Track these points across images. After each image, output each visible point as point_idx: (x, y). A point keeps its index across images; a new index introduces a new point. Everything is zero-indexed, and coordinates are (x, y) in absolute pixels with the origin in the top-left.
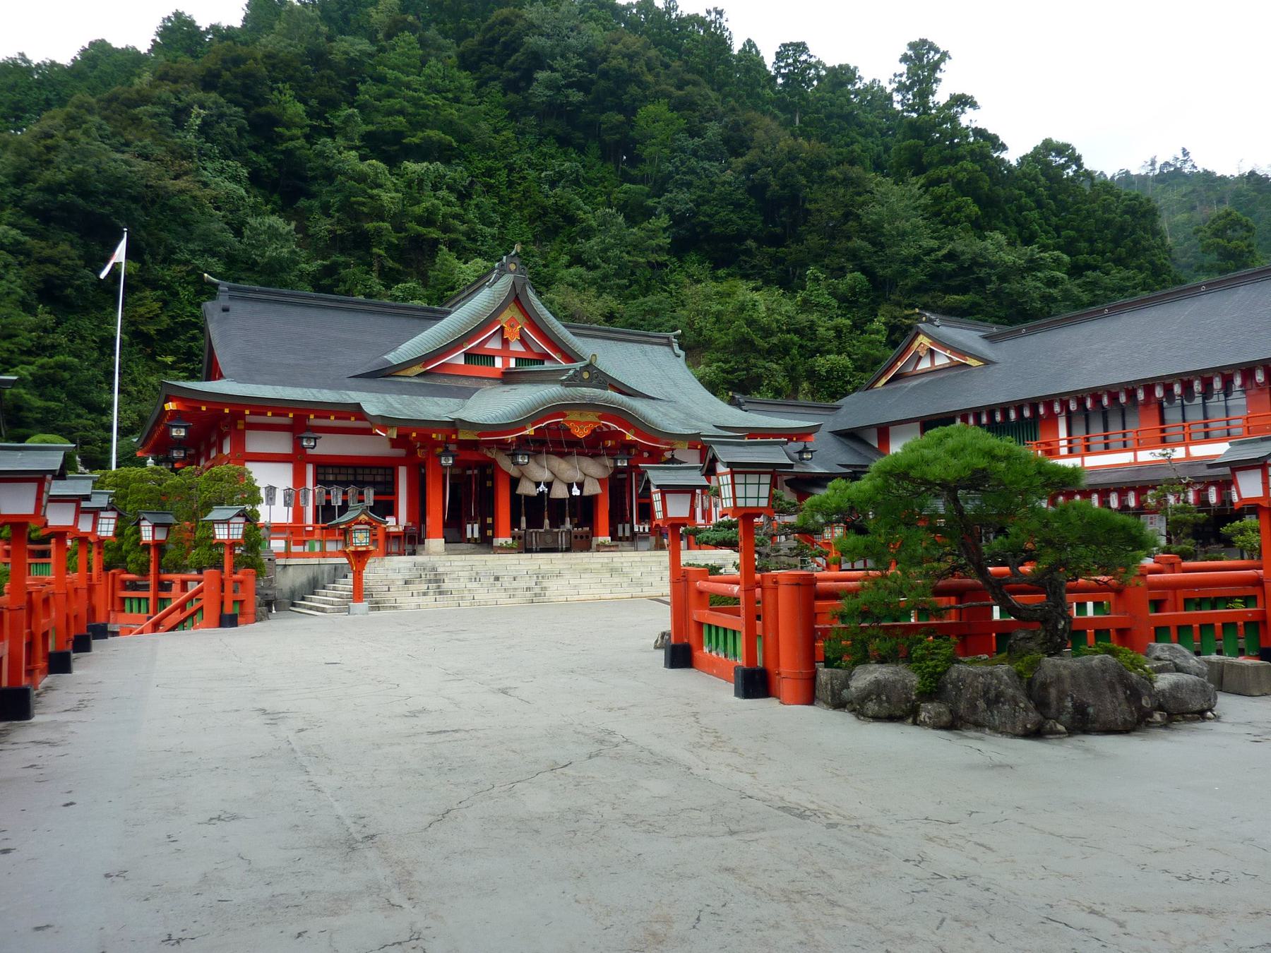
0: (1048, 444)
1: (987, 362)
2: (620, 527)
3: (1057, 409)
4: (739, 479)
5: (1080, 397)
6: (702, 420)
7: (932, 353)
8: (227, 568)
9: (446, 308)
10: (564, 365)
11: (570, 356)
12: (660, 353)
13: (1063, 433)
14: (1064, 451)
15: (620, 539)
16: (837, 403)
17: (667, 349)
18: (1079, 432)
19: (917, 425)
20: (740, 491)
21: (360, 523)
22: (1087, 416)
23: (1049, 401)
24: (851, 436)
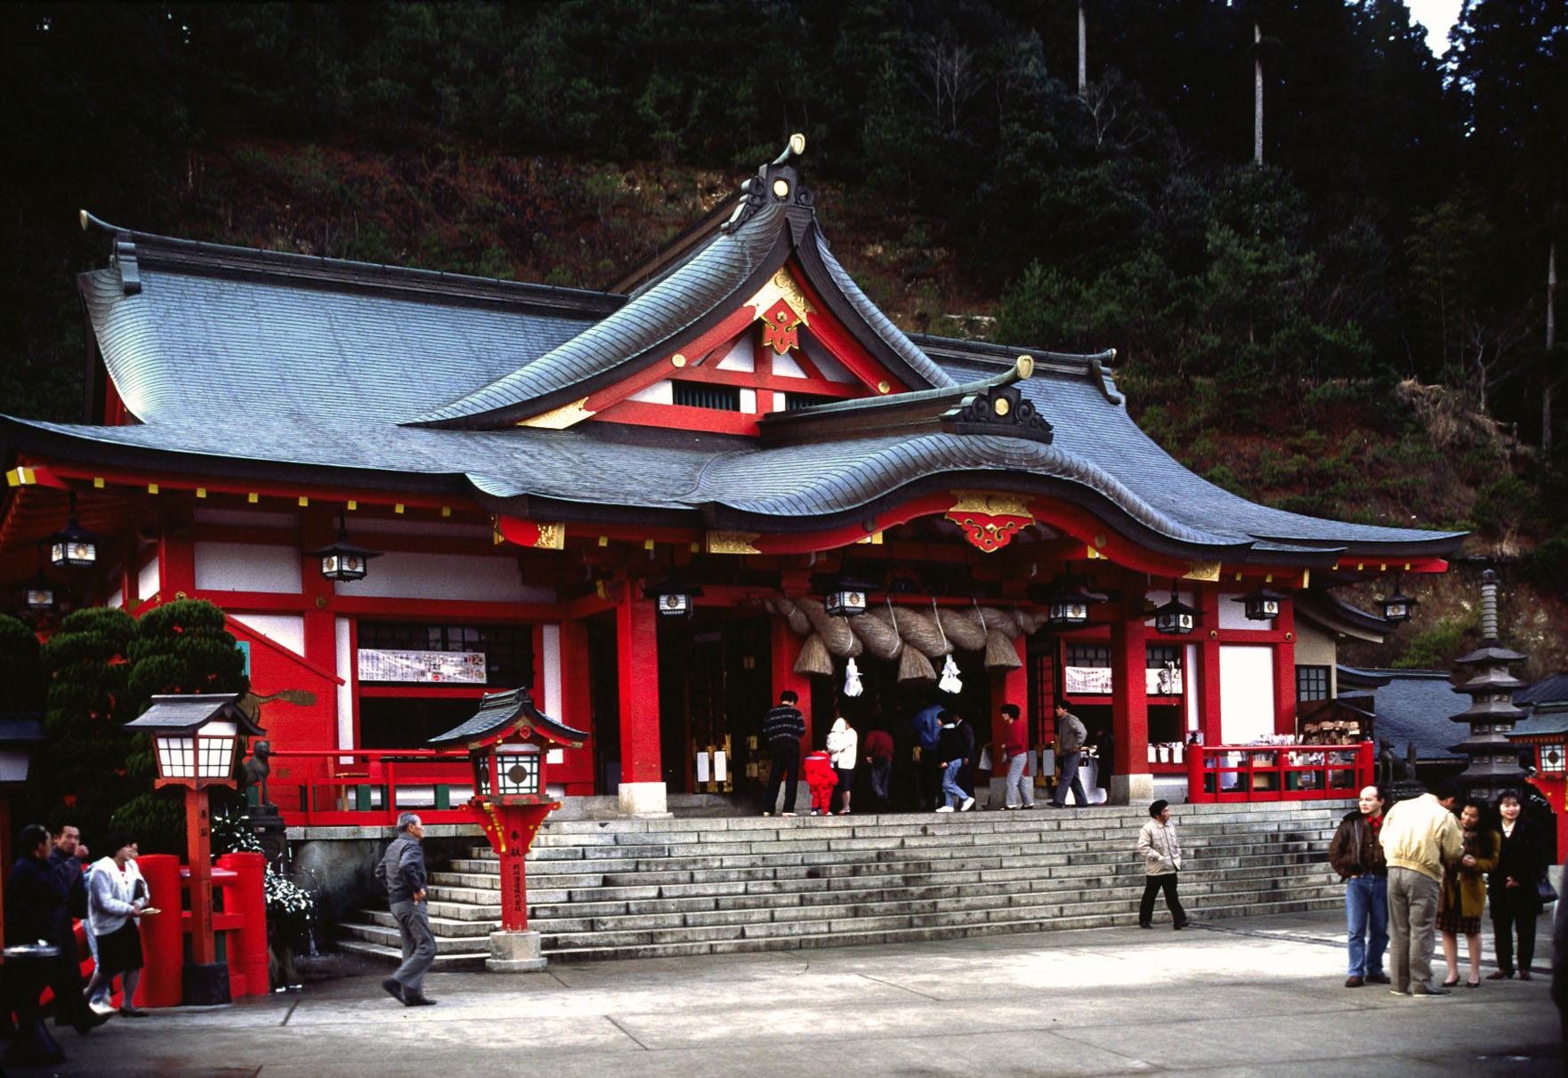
8: (196, 843)
9: (615, 293)
17: (1090, 389)
21: (516, 739)
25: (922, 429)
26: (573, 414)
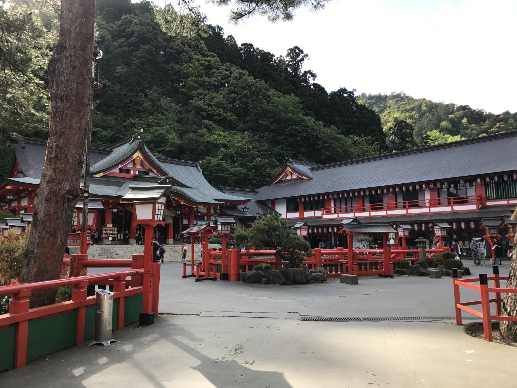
0: (328, 209)
1: (310, 179)
2: (176, 235)
3: (330, 197)
4: (223, 226)
5: (338, 193)
6: (208, 197)
7: (292, 174)
10: (160, 176)
11: (162, 172)
12: (193, 169)
13: (333, 206)
14: (333, 212)
15: (176, 240)
16: (258, 190)
17: (195, 168)
18: (338, 206)
19: (285, 200)
20: (223, 229)
22: (340, 200)
23: (328, 194)
24: (262, 203)
25: (156, 182)
26: (101, 174)
